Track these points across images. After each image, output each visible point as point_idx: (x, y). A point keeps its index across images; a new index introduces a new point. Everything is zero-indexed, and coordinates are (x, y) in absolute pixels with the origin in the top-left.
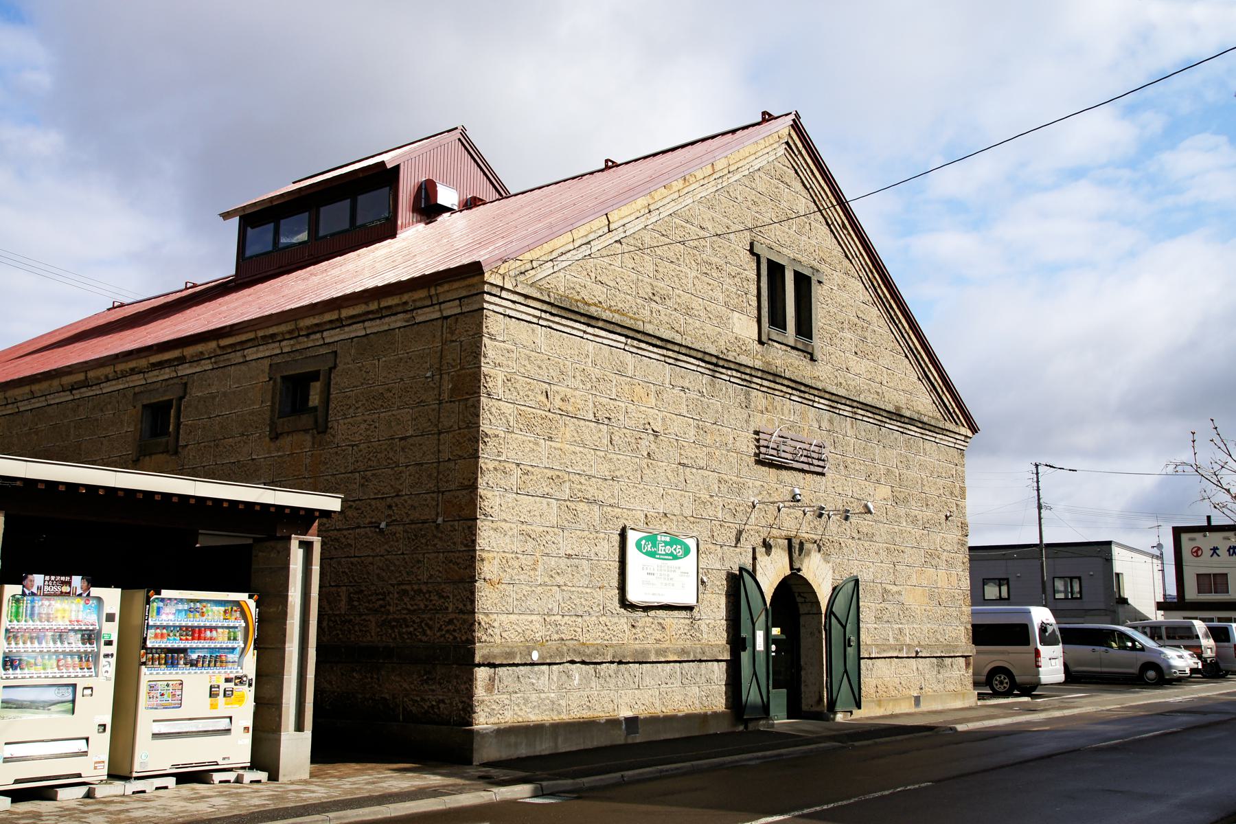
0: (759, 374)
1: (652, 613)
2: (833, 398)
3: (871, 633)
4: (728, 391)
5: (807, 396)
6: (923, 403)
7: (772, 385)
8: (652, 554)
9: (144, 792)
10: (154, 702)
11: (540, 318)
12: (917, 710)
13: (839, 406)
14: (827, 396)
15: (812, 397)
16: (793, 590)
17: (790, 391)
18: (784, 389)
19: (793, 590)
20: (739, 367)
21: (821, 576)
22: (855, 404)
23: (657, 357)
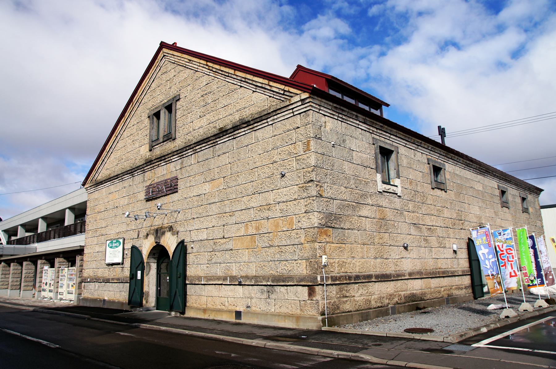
0: (145, 165)
1: (114, 266)
2: (179, 152)
3: (193, 270)
4: (128, 181)
5: (167, 160)
6: (102, 173)
7: (152, 166)
8: (111, 247)
9: (431, 331)
10: (26, 284)
11: (201, 148)
12: (238, 321)
13: (184, 153)
14: (175, 153)
15: (169, 159)
16: (159, 252)
17: (159, 163)
18: (157, 164)
19: (159, 252)
20: (138, 168)
21: (170, 243)
22: (192, 146)
23: (249, 131)
